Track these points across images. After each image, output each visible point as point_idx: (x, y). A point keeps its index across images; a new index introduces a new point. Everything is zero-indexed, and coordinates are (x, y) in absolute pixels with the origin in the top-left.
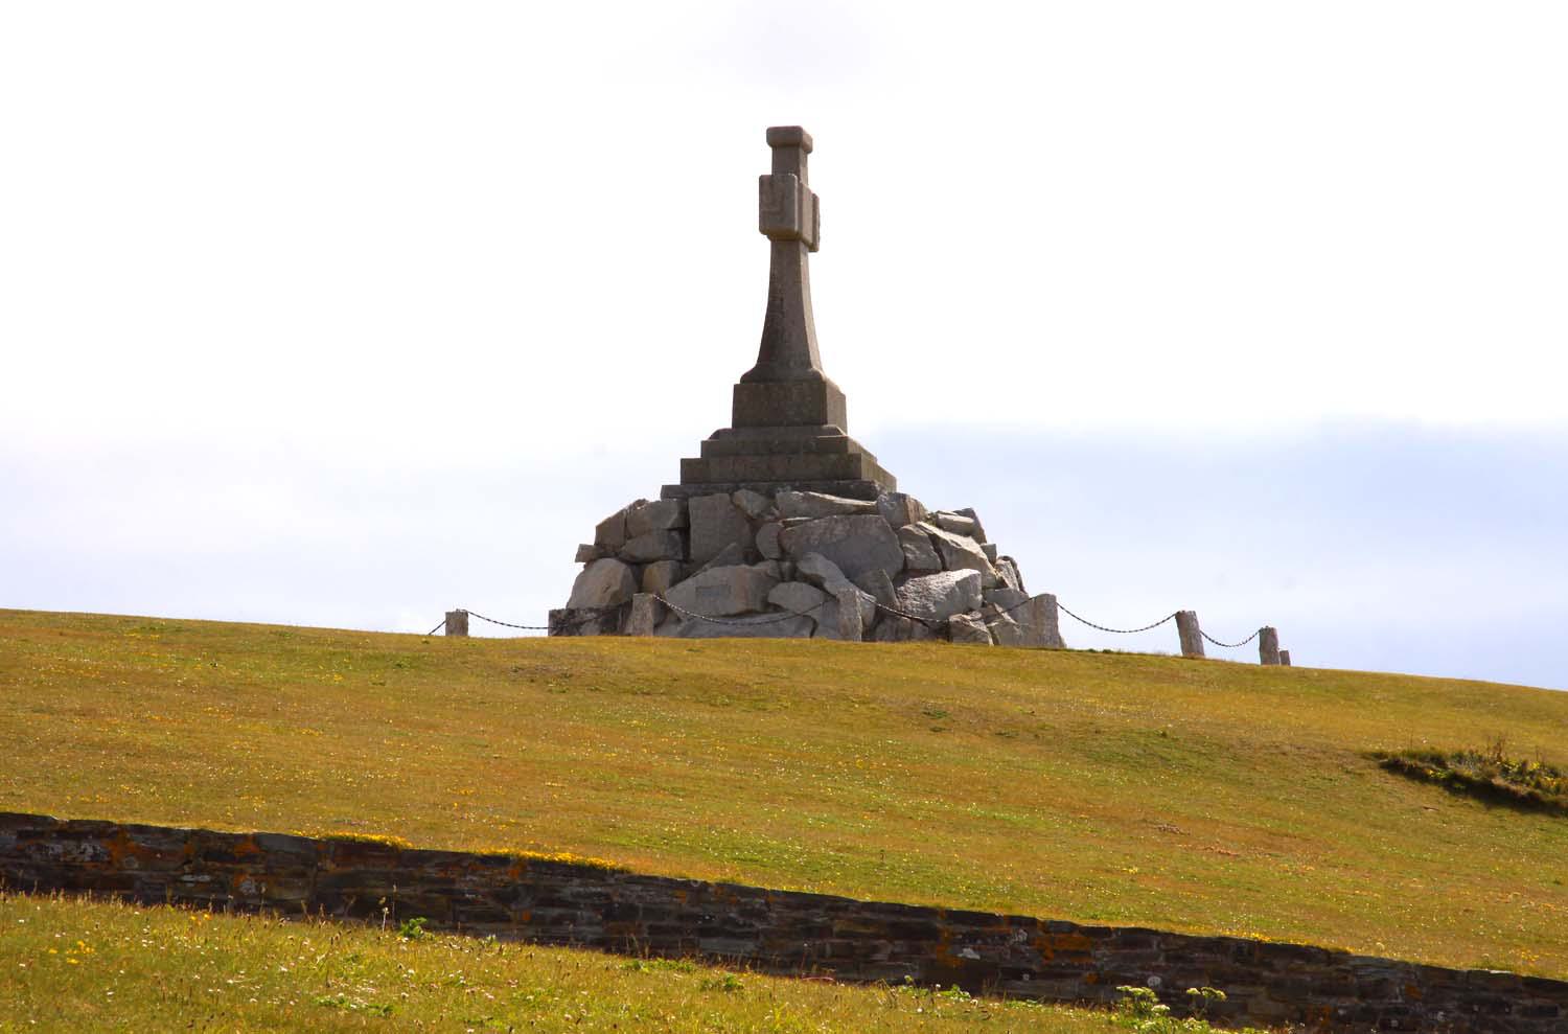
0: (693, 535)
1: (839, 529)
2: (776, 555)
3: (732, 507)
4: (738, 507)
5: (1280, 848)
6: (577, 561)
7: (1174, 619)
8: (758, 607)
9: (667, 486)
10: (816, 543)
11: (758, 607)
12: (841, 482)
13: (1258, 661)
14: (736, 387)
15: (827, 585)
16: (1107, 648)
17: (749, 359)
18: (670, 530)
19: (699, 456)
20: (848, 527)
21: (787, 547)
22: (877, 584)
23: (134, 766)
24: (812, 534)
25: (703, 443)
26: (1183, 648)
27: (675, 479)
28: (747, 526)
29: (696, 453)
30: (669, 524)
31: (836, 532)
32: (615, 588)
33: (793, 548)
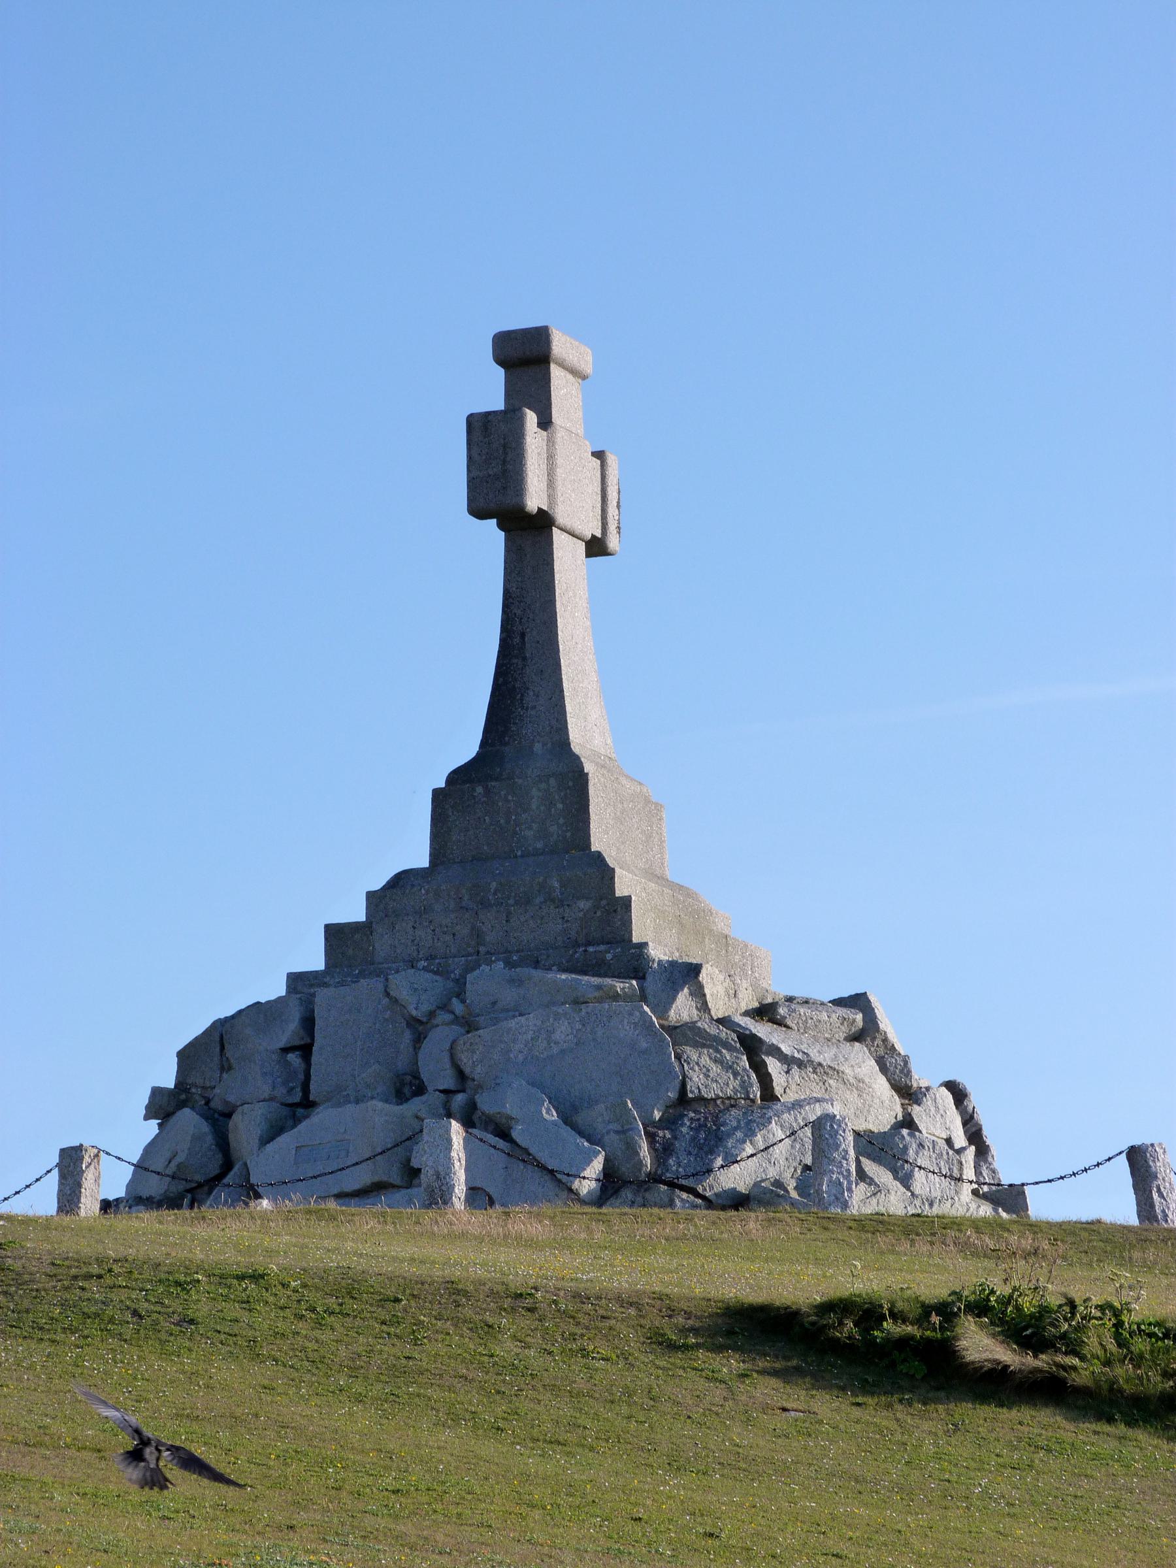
0: (315, 1058)
1: (563, 1032)
2: (449, 1082)
3: (386, 1001)
4: (395, 1001)
5: (983, 1222)
6: (146, 1118)
7: (1123, 1161)
8: (396, 1179)
9: (291, 973)
10: (521, 1057)
11: (396, 1179)
12: (591, 949)
13: (1134, 1221)
14: (437, 794)
15: (515, 1135)
16: (790, 993)
17: (467, 747)
18: (286, 1050)
19: (363, 919)
20: (578, 1026)
21: (467, 1070)
22: (615, 1126)
23: (228, 1348)
24: (514, 1041)
25: (370, 896)
26: (1139, 1216)
27: (314, 959)
28: (408, 1036)
29: (358, 914)
30: (283, 1040)
31: (557, 1036)
32: (180, 1158)
33: (478, 1069)
